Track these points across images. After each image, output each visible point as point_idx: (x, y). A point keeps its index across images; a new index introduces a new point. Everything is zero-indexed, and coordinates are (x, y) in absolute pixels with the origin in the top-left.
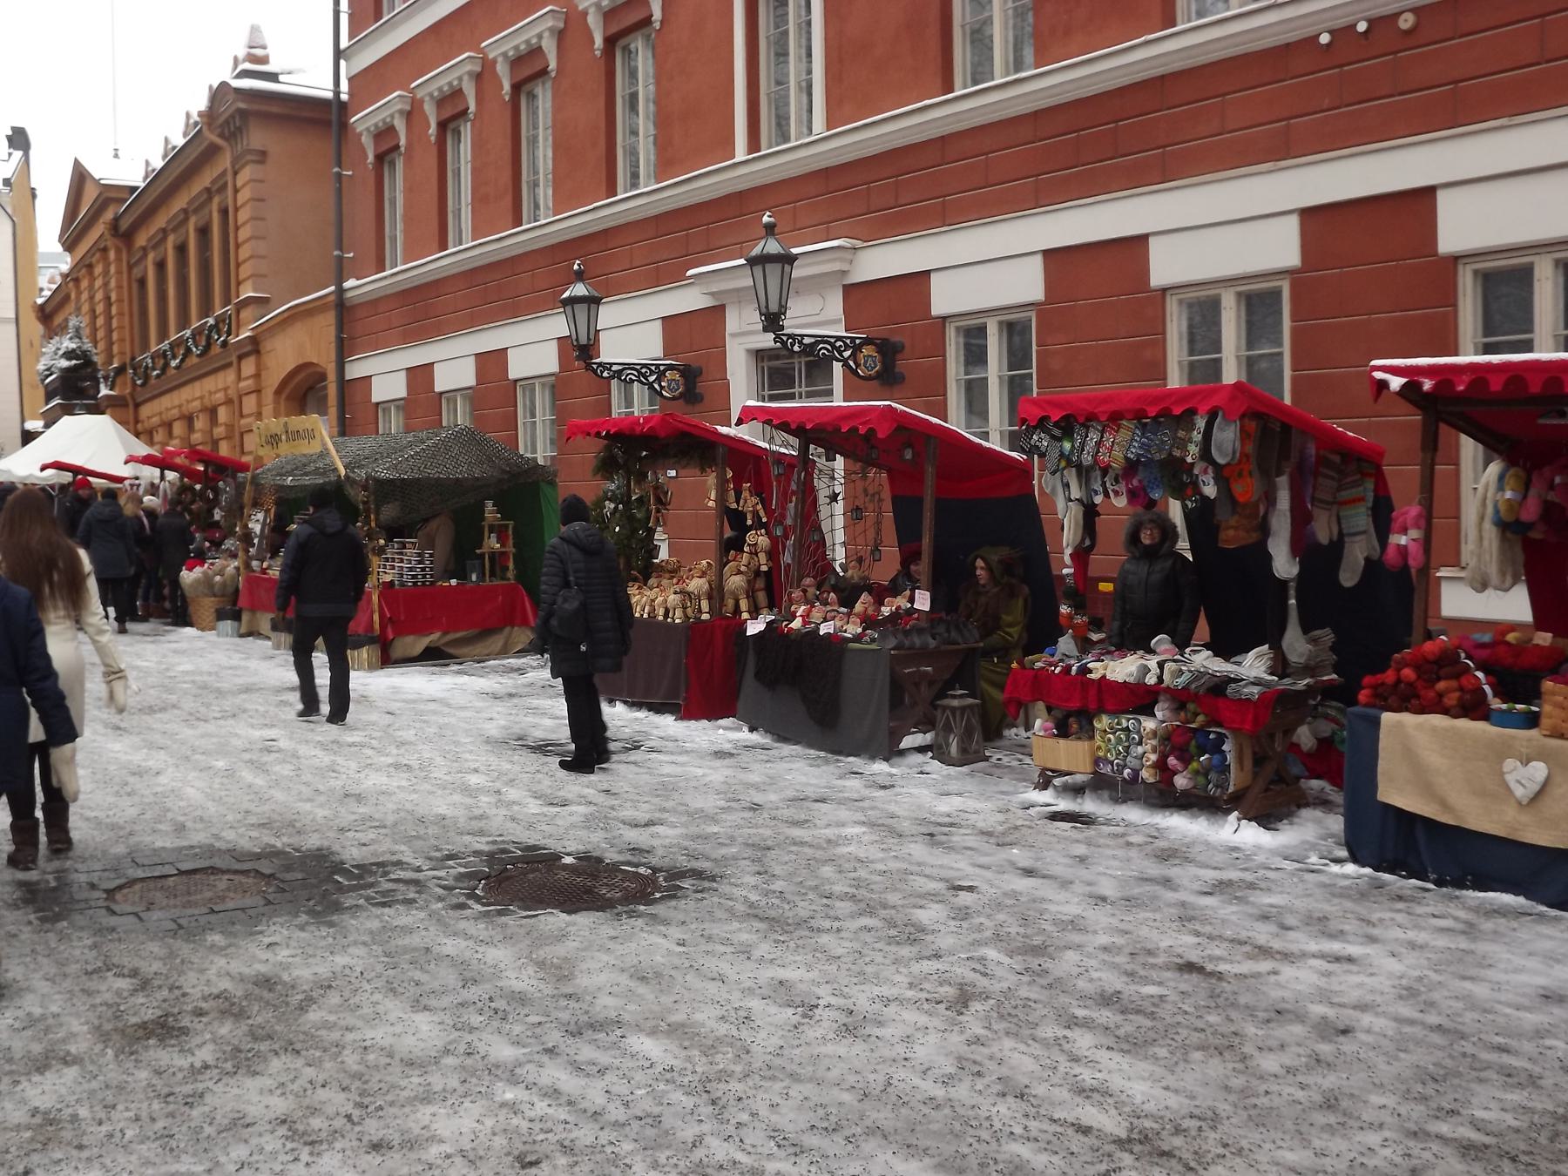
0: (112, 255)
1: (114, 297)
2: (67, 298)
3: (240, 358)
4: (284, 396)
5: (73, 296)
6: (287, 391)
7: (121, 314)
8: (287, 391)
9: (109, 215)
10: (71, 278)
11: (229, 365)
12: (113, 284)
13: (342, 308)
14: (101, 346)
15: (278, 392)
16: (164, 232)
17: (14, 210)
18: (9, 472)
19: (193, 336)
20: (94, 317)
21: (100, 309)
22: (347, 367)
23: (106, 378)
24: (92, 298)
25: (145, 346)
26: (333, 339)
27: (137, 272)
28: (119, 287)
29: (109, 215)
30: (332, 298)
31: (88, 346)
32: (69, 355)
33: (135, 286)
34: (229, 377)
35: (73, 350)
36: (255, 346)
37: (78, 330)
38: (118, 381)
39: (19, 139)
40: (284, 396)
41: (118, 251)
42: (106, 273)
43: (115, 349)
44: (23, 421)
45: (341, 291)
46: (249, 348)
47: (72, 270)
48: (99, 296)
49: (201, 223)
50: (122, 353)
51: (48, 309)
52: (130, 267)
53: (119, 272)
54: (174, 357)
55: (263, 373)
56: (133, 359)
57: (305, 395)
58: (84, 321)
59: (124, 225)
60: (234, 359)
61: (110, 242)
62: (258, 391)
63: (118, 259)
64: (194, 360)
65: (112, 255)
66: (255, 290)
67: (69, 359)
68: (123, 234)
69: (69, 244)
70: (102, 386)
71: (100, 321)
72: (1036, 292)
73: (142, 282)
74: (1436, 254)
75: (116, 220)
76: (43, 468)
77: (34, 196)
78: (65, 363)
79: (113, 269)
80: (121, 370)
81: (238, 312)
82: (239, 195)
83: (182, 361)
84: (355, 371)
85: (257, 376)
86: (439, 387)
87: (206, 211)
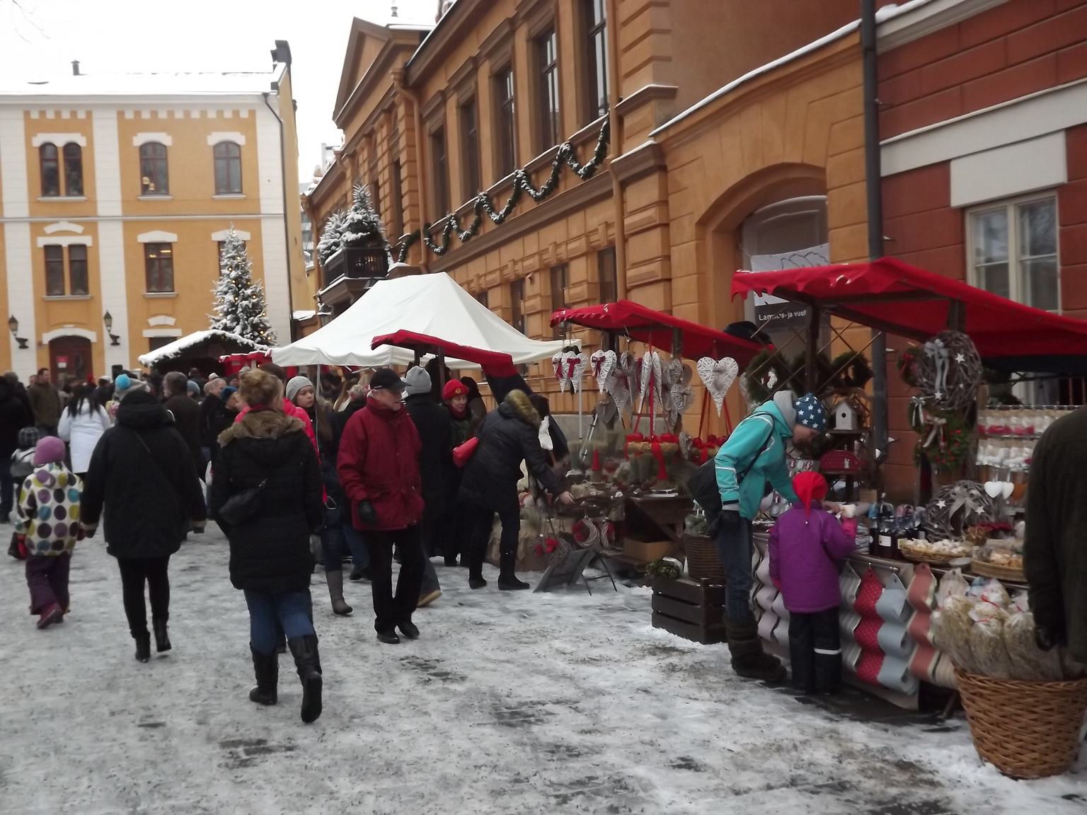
0: (401, 111)
1: (403, 158)
2: (342, 177)
3: (624, 185)
4: (712, 227)
5: (349, 173)
6: (721, 217)
7: (412, 176)
8: (721, 217)
9: (398, 64)
10: (348, 155)
11: (609, 195)
12: (402, 143)
13: (874, 53)
14: (387, 216)
15: (703, 223)
16: (475, 62)
17: (281, 112)
18: (319, 352)
19: (527, 174)
20: (376, 186)
21: (384, 177)
22: (885, 156)
23: (395, 252)
24: (372, 169)
25: (443, 203)
26: (859, 107)
27: (431, 126)
28: (410, 146)
29: (398, 64)
30: (855, 39)
31: (373, 217)
32: (355, 227)
33: (428, 143)
34: (608, 211)
35: (360, 221)
36: (658, 161)
37: (362, 200)
38: (410, 252)
39: (282, 52)
40: (712, 227)
41: (409, 105)
42: (393, 134)
43: (406, 216)
44: (292, 313)
45: (872, 26)
46: (651, 163)
47: (347, 148)
48: (384, 162)
49: (434, 129)
50: (414, 220)
51: (316, 200)
52: (422, 122)
53: (410, 129)
54: (493, 210)
55: (671, 199)
56: (427, 225)
57: (740, 227)
58: (365, 189)
59: (416, 73)
60: (615, 186)
61: (401, 94)
62: (665, 225)
63: (409, 114)
64: (528, 205)
65: (401, 111)
66: (656, 80)
67: (355, 231)
68: (414, 85)
69: (343, 120)
70: (390, 260)
71: (385, 190)
72: (1058, 175)
73: (439, 137)
74: (949, 205)
75: (407, 69)
76: (374, 346)
77: (295, 108)
78: (350, 236)
79: (402, 127)
80: (414, 239)
81: (620, 121)
82: (381, 191)
83: (508, 212)
84: (903, 157)
85: (663, 203)
86: (958, 198)
87: (440, 115)
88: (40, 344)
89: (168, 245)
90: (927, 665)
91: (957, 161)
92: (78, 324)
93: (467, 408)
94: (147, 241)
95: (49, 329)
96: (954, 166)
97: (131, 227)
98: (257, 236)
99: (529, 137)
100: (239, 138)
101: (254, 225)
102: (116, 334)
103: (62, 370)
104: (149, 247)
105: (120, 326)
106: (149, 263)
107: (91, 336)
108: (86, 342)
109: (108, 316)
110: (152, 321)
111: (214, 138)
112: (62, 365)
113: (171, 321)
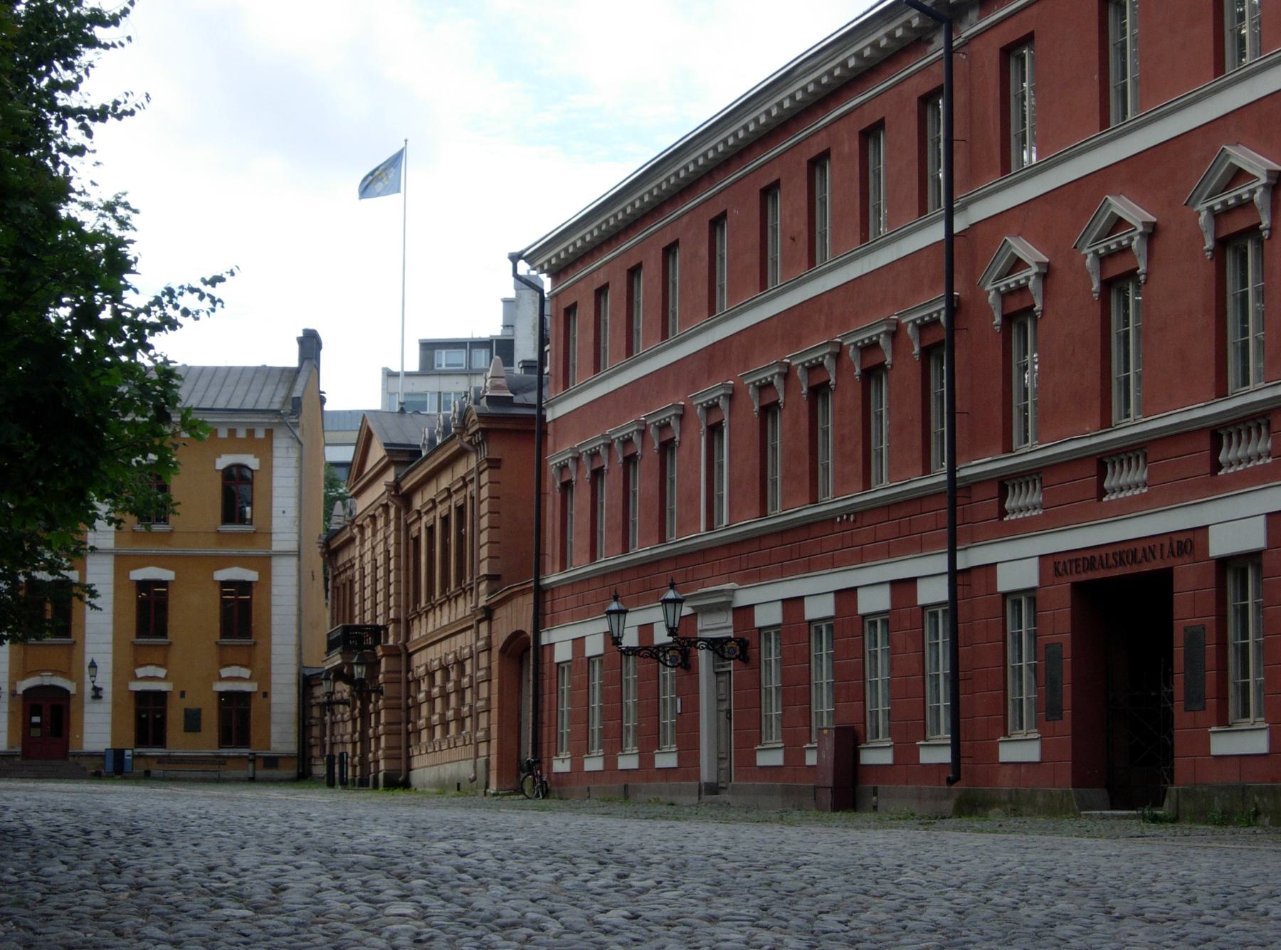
22: (959, 556)
88: (13, 693)
89: (164, 584)
90: (387, 665)
91: (927, 581)
92: (56, 672)
93: (116, 313)
94: (140, 578)
95: (27, 674)
96: (860, 591)
97: (123, 562)
98: (266, 573)
99: (168, 726)
100: (252, 461)
101: (264, 563)
102: (98, 685)
103: (36, 725)
104: (143, 585)
105: (104, 678)
106: (142, 606)
107: (71, 687)
108: (65, 692)
109: (93, 665)
110: (140, 672)
111: (223, 462)
112: (36, 719)
113: (161, 673)
